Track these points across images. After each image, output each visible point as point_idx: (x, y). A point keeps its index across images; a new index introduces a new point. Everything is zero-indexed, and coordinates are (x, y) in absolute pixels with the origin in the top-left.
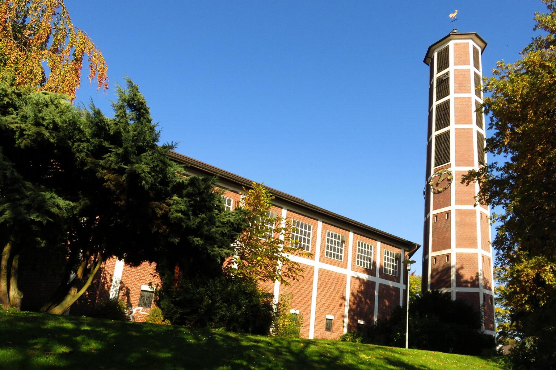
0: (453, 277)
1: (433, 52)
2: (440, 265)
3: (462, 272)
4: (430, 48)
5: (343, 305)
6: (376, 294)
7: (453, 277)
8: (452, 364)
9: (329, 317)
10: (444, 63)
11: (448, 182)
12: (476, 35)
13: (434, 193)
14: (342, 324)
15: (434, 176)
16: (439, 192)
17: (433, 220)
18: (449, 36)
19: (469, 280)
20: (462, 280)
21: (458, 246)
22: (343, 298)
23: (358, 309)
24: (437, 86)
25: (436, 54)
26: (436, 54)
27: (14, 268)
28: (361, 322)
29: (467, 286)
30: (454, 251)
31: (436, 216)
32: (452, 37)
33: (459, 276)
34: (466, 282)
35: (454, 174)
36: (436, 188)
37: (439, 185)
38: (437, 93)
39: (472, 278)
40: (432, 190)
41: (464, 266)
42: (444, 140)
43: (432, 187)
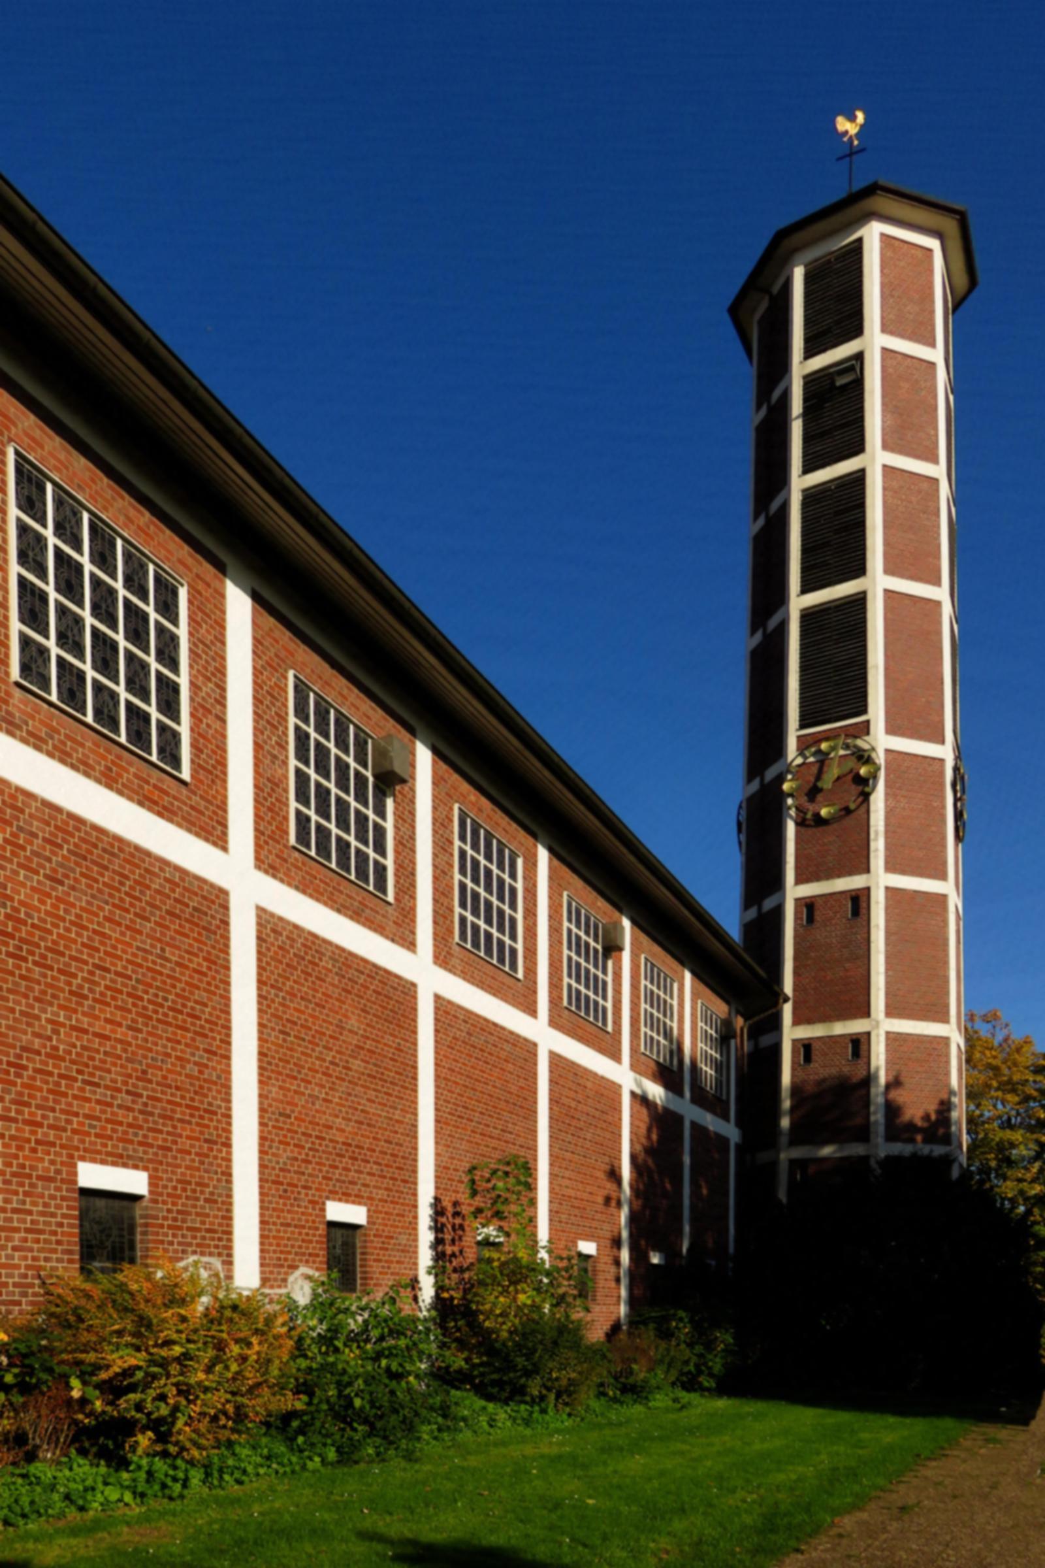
0: (878, 1117)
1: (786, 263)
2: (821, 1069)
3: (898, 1096)
4: (781, 235)
5: (613, 1203)
6: (687, 1160)
7: (878, 1117)
8: (494, 1304)
9: (339, 1211)
10: (839, 315)
11: (855, 789)
12: (962, 219)
13: (800, 823)
14: (613, 1269)
15: (799, 761)
16: (819, 821)
17: (797, 918)
18: (872, 190)
19: (920, 1123)
20: (898, 1121)
21: (892, 1011)
22: (614, 1175)
23: (647, 1213)
24: (807, 414)
25: (799, 274)
26: (799, 274)
27: (791, 817)
28: (655, 1259)
29: (912, 1140)
30: (882, 1026)
31: (808, 907)
32: (881, 202)
33: (892, 1110)
34: (911, 1127)
35: (880, 758)
36: (811, 808)
37: (820, 797)
38: (807, 439)
39: (926, 1117)
40: (793, 812)
41: (902, 1079)
42: (839, 630)
43: (790, 801)
